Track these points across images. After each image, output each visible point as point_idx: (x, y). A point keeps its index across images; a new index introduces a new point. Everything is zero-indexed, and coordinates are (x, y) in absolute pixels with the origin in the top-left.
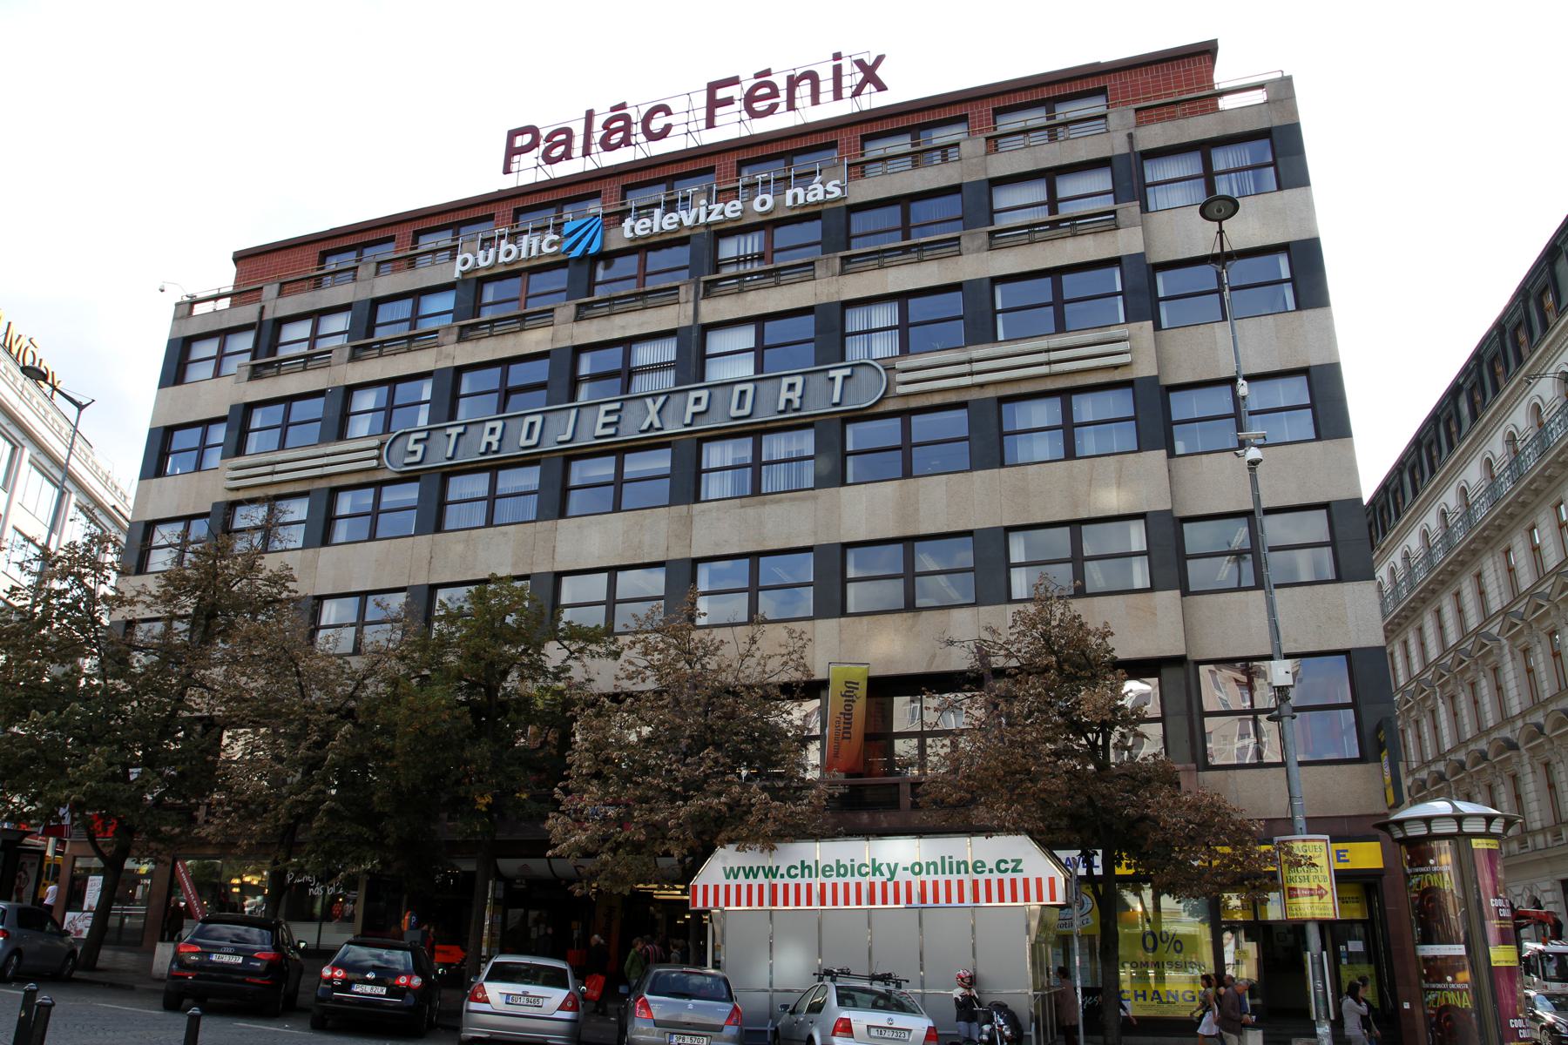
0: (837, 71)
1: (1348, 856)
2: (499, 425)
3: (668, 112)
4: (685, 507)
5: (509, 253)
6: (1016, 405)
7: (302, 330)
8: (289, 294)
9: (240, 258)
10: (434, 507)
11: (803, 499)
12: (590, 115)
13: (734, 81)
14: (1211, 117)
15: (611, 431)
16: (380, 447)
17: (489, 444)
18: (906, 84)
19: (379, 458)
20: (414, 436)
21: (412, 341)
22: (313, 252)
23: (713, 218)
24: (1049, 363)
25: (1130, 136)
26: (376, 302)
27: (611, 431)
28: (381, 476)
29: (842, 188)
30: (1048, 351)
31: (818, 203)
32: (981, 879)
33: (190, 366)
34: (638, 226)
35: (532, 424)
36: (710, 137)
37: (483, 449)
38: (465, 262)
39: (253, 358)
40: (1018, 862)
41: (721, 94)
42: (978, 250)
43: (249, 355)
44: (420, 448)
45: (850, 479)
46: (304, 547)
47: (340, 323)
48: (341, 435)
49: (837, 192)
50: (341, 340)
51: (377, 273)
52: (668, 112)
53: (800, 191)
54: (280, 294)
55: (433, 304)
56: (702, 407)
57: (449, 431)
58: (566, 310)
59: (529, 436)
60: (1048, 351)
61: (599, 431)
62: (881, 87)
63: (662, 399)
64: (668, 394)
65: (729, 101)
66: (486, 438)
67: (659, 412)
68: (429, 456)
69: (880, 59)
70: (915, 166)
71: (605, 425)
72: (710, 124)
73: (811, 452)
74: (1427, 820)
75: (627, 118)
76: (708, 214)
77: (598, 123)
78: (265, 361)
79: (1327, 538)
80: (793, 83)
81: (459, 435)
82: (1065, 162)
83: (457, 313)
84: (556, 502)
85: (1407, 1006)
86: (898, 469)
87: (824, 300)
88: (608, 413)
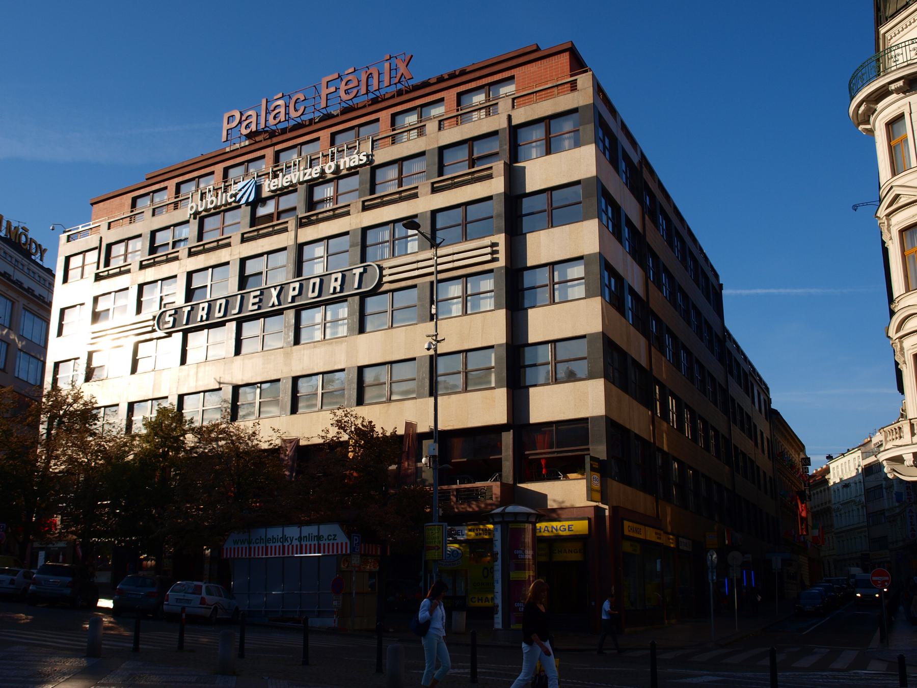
2: (297, 285)
5: (212, 202)
6: (537, 270)
8: (520, 106)
15: (256, 307)
17: (335, 288)
23: (307, 178)
24: (453, 261)
25: (510, 117)
30: (454, 254)
31: (356, 167)
32: (322, 543)
33: (519, 148)
34: (272, 184)
35: (314, 284)
39: (98, 268)
40: (335, 535)
42: (426, 194)
44: (171, 319)
45: (557, 300)
51: (153, 215)
53: (347, 159)
57: (354, 271)
58: (424, 188)
59: (313, 291)
60: (454, 254)
61: (251, 307)
63: (278, 288)
67: (278, 296)
70: (488, 114)
71: (254, 304)
73: (346, 316)
74: (516, 514)
82: (476, 134)
87: (354, 227)
88: (255, 297)
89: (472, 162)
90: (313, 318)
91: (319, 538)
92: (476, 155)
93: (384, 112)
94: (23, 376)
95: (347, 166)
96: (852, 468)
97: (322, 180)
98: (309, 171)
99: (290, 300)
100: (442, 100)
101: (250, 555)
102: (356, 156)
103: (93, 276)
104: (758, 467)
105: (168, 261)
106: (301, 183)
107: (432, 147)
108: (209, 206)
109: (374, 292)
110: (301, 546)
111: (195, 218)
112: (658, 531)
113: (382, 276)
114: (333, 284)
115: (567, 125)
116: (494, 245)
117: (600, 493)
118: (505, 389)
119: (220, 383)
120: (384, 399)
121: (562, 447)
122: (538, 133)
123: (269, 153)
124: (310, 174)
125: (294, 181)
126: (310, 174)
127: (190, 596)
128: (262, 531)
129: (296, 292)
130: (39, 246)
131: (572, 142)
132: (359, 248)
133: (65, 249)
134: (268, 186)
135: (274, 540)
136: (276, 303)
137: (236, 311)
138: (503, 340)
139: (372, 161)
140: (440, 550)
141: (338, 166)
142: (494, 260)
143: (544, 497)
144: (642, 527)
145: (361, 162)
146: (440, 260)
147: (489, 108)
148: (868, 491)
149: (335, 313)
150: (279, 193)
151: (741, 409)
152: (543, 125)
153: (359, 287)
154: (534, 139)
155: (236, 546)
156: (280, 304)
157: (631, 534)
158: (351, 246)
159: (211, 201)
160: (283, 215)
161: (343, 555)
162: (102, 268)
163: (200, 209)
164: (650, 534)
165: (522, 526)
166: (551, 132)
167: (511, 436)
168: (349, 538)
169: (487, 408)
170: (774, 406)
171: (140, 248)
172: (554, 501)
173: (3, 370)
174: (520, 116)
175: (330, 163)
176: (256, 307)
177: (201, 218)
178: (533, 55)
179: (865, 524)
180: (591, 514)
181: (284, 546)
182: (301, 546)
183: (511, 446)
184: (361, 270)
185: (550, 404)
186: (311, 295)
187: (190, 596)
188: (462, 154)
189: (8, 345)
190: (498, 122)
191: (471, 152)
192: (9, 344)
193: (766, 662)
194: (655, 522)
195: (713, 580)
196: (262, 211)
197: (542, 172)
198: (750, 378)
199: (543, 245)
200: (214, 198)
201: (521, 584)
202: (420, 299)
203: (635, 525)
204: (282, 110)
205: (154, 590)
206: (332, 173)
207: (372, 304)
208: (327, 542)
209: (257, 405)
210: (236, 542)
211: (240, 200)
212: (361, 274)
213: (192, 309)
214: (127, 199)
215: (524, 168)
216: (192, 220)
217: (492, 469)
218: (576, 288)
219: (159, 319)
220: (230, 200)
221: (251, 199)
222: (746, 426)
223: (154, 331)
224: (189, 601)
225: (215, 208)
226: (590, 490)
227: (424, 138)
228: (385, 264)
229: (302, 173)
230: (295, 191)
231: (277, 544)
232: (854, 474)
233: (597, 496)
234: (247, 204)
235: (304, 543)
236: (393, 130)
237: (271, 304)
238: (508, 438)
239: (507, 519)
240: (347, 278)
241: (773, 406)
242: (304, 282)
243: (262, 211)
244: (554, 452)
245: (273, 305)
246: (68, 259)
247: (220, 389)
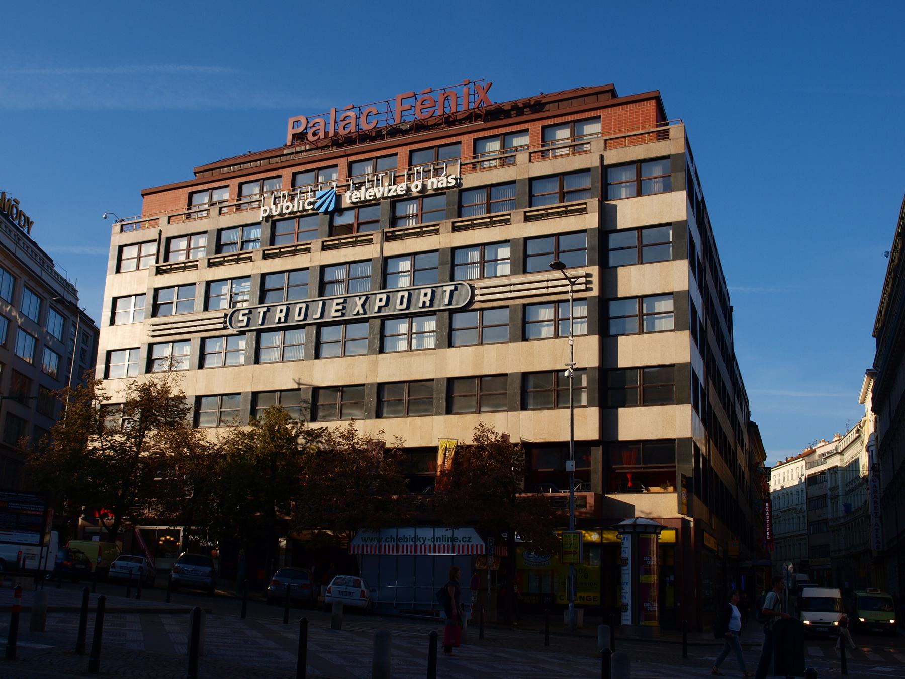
2: (384, 296)
4: (374, 356)
5: (288, 208)
7: (183, 244)
8: (612, 147)
10: (446, 333)
14: (514, 168)
15: (339, 314)
17: (280, 319)
20: (242, 312)
23: (391, 194)
24: (547, 287)
25: (602, 157)
30: (547, 281)
31: (443, 188)
32: (456, 544)
34: (354, 197)
35: (402, 297)
39: (157, 262)
42: (519, 222)
44: (245, 319)
47: (202, 241)
53: (435, 180)
57: (445, 288)
59: (401, 303)
60: (547, 281)
61: (334, 314)
63: (363, 298)
66: (422, 299)
67: (363, 305)
71: (337, 311)
76: (389, 190)
86: (340, 353)
87: (443, 246)
88: (338, 304)
89: (563, 196)
90: (397, 329)
91: (453, 539)
92: (565, 190)
93: (467, 136)
94: (20, 353)
95: (435, 187)
96: (795, 477)
97: (408, 197)
98: (393, 187)
99: (376, 310)
100: (526, 131)
101: (380, 551)
102: (445, 178)
103: (155, 269)
105: (238, 260)
106: (383, 198)
107: (522, 177)
108: (284, 211)
109: (464, 309)
110: (435, 546)
111: (267, 221)
113: (473, 295)
115: (657, 170)
116: (588, 275)
117: (686, 506)
118: (597, 409)
119: (299, 384)
120: (474, 410)
121: (653, 462)
122: (628, 175)
123: (343, 163)
124: (396, 190)
125: (378, 196)
126: (396, 190)
127: (350, 589)
128: (393, 532)
129: (383, 303)
130: (27, 219)
131: (661, 185)
133: (118, 239)
135: (405, 539)
136: (361, 312)
137: (318, 316)
138: (596, 364)
139: (461, 184)
141: (424, 186)
142: (588, 289)
143: (631, 508)
145: (449, 185)
147: (576, 148)
148: (810, 500)
149: (421, 325)
150: (359, 206)
152: (635, 166)
153: (450, 303)
154: (624, 179)
155: (365, 544)
156: (365, 313)
158: (441, 264)
159: (286, 207)
160: (362, 227)
161: (481, 555)
162: (161, 263)
163: (274, 213)
165: (648, 536)
166: (641, 177)
167: (600, 452)
168: (485, 539)
169: (587, 424)
170: (752, 419)
171: (202, 246)
172: (642, 512)
173: (4, 346)
174: (613, 157)
175: (416, 182)
176: (339, 314)
178: (607, 97)
180: (679, 526)
181: (416, 546)
182: (435, 546)
183: (600, 460)
184: (452, 288)
185: (639, 423)
186: (398, 307)
187: (350, 589)
188: (553, 187)
189: (10, 321)
191: (561, 186)
192: (10, 321)
195: (788, 587)
196: (340, 221)
197: (632, 212)
199: (634, 280)
200: (289, 204)
201: (648, 586)
202: (511, 319)
204: (353, 121)
205: (307, 582)
206: (419, 192)
207: (460, 320)
208: (462, 543)
209: (338, 406)
210: (364, 540)
211: (319, 208)
212: (452, 292)
213: (269, 310)
214: (184, 193)
215: (616, 206)
216: (264, 223)
217: (584, 478)
218: (663, 320)
219: (229, 319)
220: (307, 207)
221: (331, 209)
223: (225, 328)
224: (351, 594)
225: (289, 214)
226: (680, 503)
230: (379, 204)
231: (409, 544)
232: (796, 483)
233: (685, 509)
234: (326, 212)
235: (437, 544)
237: (355, 313)
238: (597, 454)
239: (637, 530)
240: (436, 295)
241: (752, 419)
242: (390, 294)
243: (340, 221)
244: (640, 468)
245: (358, 314)
246: (121, 248)
247: (299, 389)
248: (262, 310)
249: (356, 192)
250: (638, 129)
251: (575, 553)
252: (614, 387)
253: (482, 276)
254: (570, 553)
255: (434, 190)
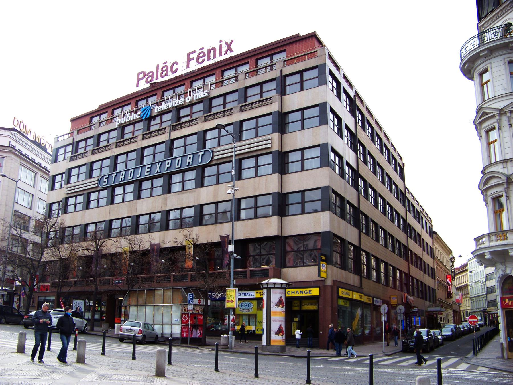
0: (221, 47)
1: (311, 292)
2: (170, 161)
3: (177, 64)
4: (165, 195)
5: (128, 118)
9: (73, 120)
11: (192, 192)
12: (158, 66)
13: (194, 52)
15: (149, 173)
16: (98, 181)
18: (238, 50)
19: (98, 184)
21: (262, 102)
22: (88, 119)
23: (177, 104)
25: (281, 70)
26: (246, 88)
27: (149, 173)
28: (99, 189)
29: (208, 93)
35: (179, 160)
36: (189, 70)
37: (187, 164)
38: (118, 122)
39: (72, 154)
41: (191, 56)
42: (237, 112)
43: (202, 112)
44: (106, 180)
46: (163, 194)
48: (240, 140)
49: (206, 94)
50: (201, 114)
51: (100, 126)
52: (177, 64)
54: (78, 134)
55: (196, 108)
56: (169, 165)
57: (199, 154)
59: (178, 165)
61: (146, 174)
62: (232, 51)
63: (160, 163)
64: (162, 162)
65: (193, 59)
66: (188, 161)
67: (160, 167)
68: (109, 183)
69: (232, 41)
71: (148, 172)
72: (188, 67)
74: (275, 284)
75: (167, 66)
77: (160, 68)
78: (75, 155)
79: (300, 201)
80: (209, 51)
81: (203, 155)
83: (204, 111)
84: (200, 183)
85: (321, 333)
87: (200, 130)
88: (148, 168)
97: (183, 107)
98: (177, 101)
102: (202, 93)
104: (424, 262)
107: (241, 87)
109: (208, 165)
111: (120, 127)
112: (361, 294)
114: (188, 161)
132: (202, 141)
134: (157, 109)
140: (234, 303)
141: (192, 99)
144: (351, 292)
146: (237, 149)
151: (415, 231)
157: (344, 296)
164: (355, 296)
174: (287, 70)
177: (122, 127)
179: (485, 293)
190: (275, 74)
193: (368, 362)
194: (359, 289)
198: (421, 214)
200: (130, 117)
203: (346, 291)
219: (100, 180)
222: (418, 239)
225: (129, 122)
227: (237, 83)
228: (215, 150)
229: (174, 102)
234: (146, 119)
236: (222, 78)
241: (434, 230)
245: (158, 172)
248: (114, 175)
249: (160, 106)
250: (302, 53)
251: (232, 301)
252: (281, 204)
253: (219, 145)
254: (228, 301)
255: (197, 100)
